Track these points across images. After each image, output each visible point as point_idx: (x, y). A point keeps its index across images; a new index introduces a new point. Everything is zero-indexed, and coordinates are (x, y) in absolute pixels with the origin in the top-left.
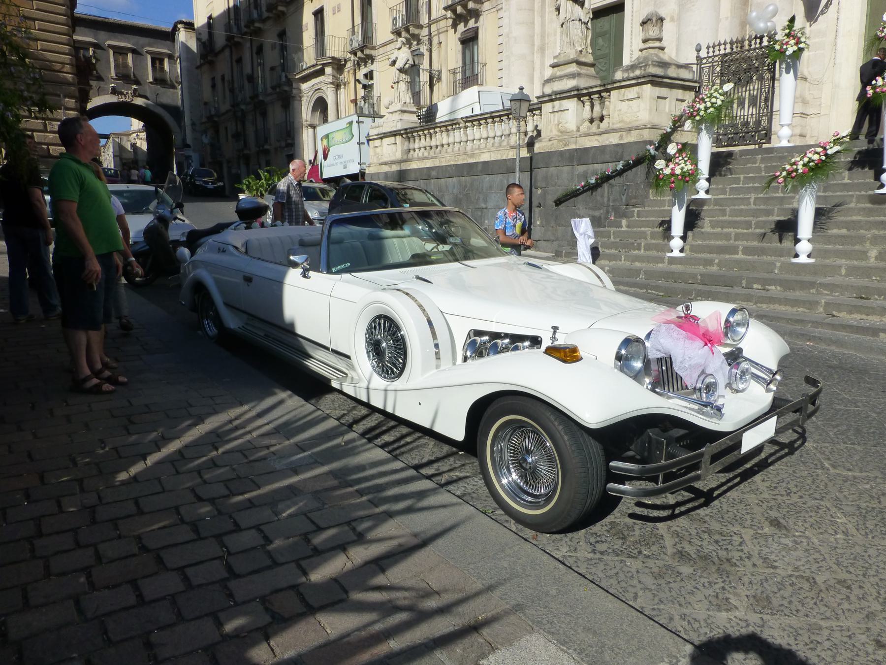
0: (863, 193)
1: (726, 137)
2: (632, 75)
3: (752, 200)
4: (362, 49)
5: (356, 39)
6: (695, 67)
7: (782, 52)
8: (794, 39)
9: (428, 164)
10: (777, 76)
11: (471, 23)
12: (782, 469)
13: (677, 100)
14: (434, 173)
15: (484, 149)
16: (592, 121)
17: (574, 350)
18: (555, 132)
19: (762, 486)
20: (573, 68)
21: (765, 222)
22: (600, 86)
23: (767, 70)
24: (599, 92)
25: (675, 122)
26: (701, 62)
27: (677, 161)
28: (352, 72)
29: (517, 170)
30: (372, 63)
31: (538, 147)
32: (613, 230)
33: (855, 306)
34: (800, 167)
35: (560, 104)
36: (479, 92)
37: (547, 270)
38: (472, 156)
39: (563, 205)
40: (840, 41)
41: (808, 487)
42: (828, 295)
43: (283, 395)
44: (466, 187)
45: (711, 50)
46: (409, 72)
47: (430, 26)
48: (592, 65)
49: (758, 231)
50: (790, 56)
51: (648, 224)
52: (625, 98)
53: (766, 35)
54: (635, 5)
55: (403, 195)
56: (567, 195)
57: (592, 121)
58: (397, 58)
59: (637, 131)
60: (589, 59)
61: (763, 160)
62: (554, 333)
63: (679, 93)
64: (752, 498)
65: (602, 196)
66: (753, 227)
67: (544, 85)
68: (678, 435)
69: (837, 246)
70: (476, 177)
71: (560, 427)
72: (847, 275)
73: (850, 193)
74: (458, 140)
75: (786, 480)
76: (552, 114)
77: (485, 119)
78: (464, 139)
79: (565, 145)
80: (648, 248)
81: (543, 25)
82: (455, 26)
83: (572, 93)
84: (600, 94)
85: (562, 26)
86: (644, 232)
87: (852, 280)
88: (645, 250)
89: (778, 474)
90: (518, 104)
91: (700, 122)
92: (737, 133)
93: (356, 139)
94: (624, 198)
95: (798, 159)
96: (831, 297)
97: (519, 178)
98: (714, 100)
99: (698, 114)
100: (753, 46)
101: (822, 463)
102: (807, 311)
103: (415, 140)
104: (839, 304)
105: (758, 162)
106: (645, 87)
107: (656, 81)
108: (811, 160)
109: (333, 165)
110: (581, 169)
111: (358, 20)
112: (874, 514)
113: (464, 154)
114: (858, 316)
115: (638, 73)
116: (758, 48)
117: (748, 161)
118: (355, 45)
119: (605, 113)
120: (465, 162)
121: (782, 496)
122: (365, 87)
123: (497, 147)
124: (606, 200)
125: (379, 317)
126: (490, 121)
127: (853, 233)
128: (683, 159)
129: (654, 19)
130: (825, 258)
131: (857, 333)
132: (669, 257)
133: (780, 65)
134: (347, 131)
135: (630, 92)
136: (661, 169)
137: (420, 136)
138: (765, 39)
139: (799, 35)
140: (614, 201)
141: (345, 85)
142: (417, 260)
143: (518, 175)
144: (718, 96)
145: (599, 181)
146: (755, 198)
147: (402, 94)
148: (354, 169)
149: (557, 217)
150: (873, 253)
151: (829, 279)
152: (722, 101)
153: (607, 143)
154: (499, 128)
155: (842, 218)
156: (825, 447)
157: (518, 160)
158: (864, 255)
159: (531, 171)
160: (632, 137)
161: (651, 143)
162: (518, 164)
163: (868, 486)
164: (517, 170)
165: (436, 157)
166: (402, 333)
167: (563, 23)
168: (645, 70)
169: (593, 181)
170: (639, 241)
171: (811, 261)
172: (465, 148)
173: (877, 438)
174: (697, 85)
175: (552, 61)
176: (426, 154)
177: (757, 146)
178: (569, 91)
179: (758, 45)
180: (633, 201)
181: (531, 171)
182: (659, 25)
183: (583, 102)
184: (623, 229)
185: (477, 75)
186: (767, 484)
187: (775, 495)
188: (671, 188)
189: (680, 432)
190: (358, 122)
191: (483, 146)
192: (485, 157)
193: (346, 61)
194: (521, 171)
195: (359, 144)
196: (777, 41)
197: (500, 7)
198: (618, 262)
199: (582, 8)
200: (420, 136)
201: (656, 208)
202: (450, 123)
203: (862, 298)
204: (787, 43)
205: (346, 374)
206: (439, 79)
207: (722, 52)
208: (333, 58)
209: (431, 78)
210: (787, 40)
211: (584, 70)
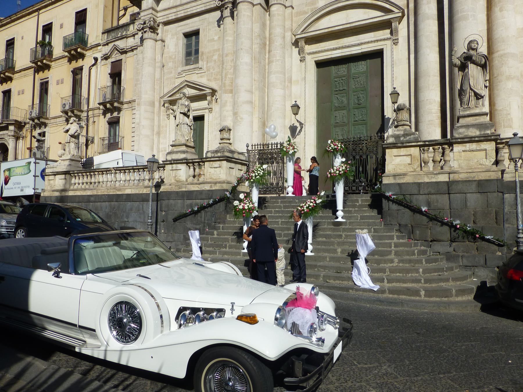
0: (329, 221)
1: (263, 190)
2: (216, 155)
3: (280, 223)
4: (38, 119)
5: (35, 112)
6: (246, 154)
7: (287, 152)
8: (292, 147)
9: (89, 193)
10: (285, 161)
11: (115, 114)
12: (338, 368)
13: (239, 170)
14: (92, 199)
15: (127, 187)
16: (194, 176)
17: (254, 317)
18: (173, 181)
19: (334, 379)
20: (184, 148)
21: (288, 234)
22: (199, 159)
23: (280, 159)
24: (198, 162)
25: (238, 181)
27: (245, 202)
28: (29, 130)
29: (151, 200)
30: (45, 127)
31: (163, 189)
32: (210, 236)
33: (336, 277)
34: (305, 209)
35: (176, 166)
36: (122, 153)
37: (207, 267)
38: (120, 190)
39: (178, 221)
40: (306, 147)
41: (353, 376)
42: (323, 271)
43: (29, 359)
44: (114, 208)
45: (254, 147)
46: (77, 137)
47: (88, 112)
48: (193, 148)
49: (285, 238)
50: (291, 155)
51: (228, 234)
52: (213, 166)
53: (279, 143)
54: (210, 118)
55: (71, 211)
56: (180, 216)
57: (194, 176)
58: (70, 129)
60: (192, 144)
61: (281, 202)
62: (233, 306)
63: (239, 167)
64: (331, 386)
65: (201, 217)
66: (283, 236)
67: (167, 155)
68: (305, 358)
69: (323, 247)
70: (122, 203)
71: (251, 362)
72: (330, 261)
73: (324, 220)
74: (110, 180)
75: (342, 374)
76: (172, 171)
77: (129, 170)
78: (114, 180)
79: (179, 188)
80: (231, 247)
81: (159, 121)
82: (104, 114)
83: (184, 161)
84: (199, 163)
85: (177, 126)
86: (228, 238)
87: (332, 264)
88: (229, 248)
89: (337, 371)
90: (152, 164)
91: (252, 183)
92: (268, 188)
93: (32, 173)
94: (213, 219)
95: (304, 205)
96: (325, 273)
97: (152, 205)
98: (259, 172)
99: (252, 179)
100: (273, 148)
101: (353, 363)
102: (315, 280)
103: (79, 178)
104: (329, 276)
105: (279, 203)
106: (223, 162)
107: (229, 160)
108: (309, 206)
109: (12, 188)
110: (189, 202)
111: (37, 101)
112: (384, 386)
113: (114, 188)
114: (338, 282)
115: (219, 154)
116: (276, 149)
117: (275, 202)
118: (34, 115)
119: (202, 173)
120: (115, 193)
121: (344, 383)
122: (38, 141)
123: (136, 186)
124: (203, 220)
125: (121, 303)
126: (132, 171)
127: (328, 240)
128: (248, 201)
129: (226, 129)
130: (318, 253)
131: (339, 290)
132: (243, 252)
133: (286, 158)
134: (26, 168)
135: (215, 164)
136: (237, 206)
137: (79, 176)
138: (279, 145)
139: (294, 145)
140: (208, 220)
141: (23, 138)
142: (129, 264)
143: (151, 203)
144: (261, 170)
145: (199, 209)
146: (281, 221)
147: (71, 150)
148: (30, 192)
149: (174, 228)
150: (339, 250)
151: (322, 263)
152: (263, 173)
153: (203, 189)
154: (136, 176)
155: (322, 233)
156: (351, 353)
157: (151, 195)
158: (335, 251)
159: (157, 201)
160: (217, 187)
161: (227, 191)
162: (151, 197)
163: (376, 372)
164: (151, 200)
165: (94, 189)
166: (138, 310)
167: (178, 125)
168: (223, 154)
169: (196, 209)
170: (225, 243)
171: (313, 254)
172: (115, 185)
173: (369, 345)
174: (247, 163)
175: (171, 143)
176: (87, 187)
177: (278, 195)
178: (182, 160)
179: (275, 148)
180: (219, 220)
181: (157, 201)
182: (229, 132)
183: (189, 167)
184: (215, 236)
185: (118, 142)
186: (335, 378)
187: (341, 383)
188: (244, 216)
189: (305, 356)
190: (35, 163)
191: (127, 185)
192: (128, 191)
193: (25, 124)
194: (152, 201)
195: (35, 176)
196: (284, 147)
197: (134, 108)
198: (215, 255)
199: (188, 119)
200: (83, 176)
201: (232, 225)
202: (105, 170)
203: (338, 272)
204: (289, 148)
205: (85, 342)
206: (93, 142)
207: (259, 148)
208: (16, 121)
209: (87, 141)
210: (289, 147)
211: (190, 150)
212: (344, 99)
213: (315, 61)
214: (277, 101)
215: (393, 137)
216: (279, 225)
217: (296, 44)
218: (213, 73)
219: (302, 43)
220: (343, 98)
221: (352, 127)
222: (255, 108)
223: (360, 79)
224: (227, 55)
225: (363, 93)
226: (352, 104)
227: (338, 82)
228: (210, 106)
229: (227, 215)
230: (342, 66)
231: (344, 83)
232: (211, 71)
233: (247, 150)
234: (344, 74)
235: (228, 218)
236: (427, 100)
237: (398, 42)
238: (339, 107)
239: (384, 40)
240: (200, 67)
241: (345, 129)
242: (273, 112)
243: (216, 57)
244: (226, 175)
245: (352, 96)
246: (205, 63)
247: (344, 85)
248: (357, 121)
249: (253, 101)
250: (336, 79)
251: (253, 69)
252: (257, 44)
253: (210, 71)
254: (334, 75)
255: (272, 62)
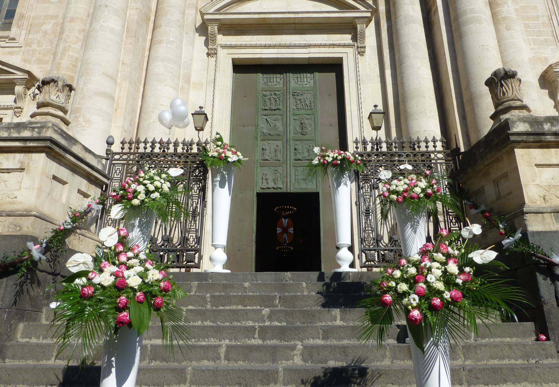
2: (15, 135)
3: (223, 351)
26: (113, 157)
27: (123, 258)
45: (127, 146)
59: (11, 219)
63: (84, 184)
115: (26, 134)
129: (60, 84)
133: (213, 177)
161: (35, 240)
168: (39, 133)
177: (183, 270)
207: (141, 150)
212: (279, 124)
213: (233, 60)
214: (162, 105)
215: (524, 122)
216: (219, 359)
217: (202, 29)
218: (36, 50)
219: (213, 28)
220: (276, 122)
221: (292, 169)
222: (119, 110)
223: (305, 97)
224: (72, 20)
225: (311, 119)
226: (292, 132)
227: (269, 97)
228: (19, 104)
229: (17, 325)
230: (275, 75)
231: (278, 100)
232: (34, 46)
233: (107, 150)
234: (278, 86)
235: (19, 335)
236: (425, 131)
237: (364, 52)
238: (269, 134)
239: (344, 46)
240: (12, 36)
241: (280, 172)
242: (154, 122)
243: (48, 27)
244: (38, 197)
245: (292, 120)
246: (24, 32)
247: (278, 102)
248: (299, 160)
249: (116, 98)
250: (264, 93)
251: (123, 46)
252: (136, 9)
253: (30, 46)
254: (262, 87)
255: (160, 42)
